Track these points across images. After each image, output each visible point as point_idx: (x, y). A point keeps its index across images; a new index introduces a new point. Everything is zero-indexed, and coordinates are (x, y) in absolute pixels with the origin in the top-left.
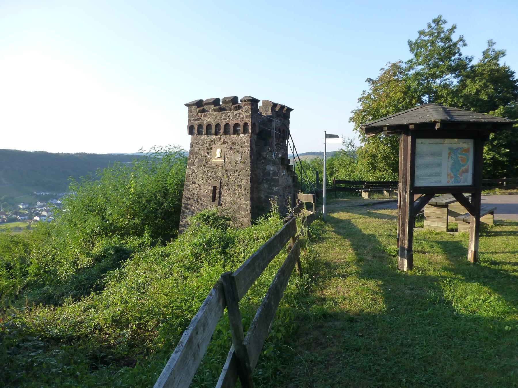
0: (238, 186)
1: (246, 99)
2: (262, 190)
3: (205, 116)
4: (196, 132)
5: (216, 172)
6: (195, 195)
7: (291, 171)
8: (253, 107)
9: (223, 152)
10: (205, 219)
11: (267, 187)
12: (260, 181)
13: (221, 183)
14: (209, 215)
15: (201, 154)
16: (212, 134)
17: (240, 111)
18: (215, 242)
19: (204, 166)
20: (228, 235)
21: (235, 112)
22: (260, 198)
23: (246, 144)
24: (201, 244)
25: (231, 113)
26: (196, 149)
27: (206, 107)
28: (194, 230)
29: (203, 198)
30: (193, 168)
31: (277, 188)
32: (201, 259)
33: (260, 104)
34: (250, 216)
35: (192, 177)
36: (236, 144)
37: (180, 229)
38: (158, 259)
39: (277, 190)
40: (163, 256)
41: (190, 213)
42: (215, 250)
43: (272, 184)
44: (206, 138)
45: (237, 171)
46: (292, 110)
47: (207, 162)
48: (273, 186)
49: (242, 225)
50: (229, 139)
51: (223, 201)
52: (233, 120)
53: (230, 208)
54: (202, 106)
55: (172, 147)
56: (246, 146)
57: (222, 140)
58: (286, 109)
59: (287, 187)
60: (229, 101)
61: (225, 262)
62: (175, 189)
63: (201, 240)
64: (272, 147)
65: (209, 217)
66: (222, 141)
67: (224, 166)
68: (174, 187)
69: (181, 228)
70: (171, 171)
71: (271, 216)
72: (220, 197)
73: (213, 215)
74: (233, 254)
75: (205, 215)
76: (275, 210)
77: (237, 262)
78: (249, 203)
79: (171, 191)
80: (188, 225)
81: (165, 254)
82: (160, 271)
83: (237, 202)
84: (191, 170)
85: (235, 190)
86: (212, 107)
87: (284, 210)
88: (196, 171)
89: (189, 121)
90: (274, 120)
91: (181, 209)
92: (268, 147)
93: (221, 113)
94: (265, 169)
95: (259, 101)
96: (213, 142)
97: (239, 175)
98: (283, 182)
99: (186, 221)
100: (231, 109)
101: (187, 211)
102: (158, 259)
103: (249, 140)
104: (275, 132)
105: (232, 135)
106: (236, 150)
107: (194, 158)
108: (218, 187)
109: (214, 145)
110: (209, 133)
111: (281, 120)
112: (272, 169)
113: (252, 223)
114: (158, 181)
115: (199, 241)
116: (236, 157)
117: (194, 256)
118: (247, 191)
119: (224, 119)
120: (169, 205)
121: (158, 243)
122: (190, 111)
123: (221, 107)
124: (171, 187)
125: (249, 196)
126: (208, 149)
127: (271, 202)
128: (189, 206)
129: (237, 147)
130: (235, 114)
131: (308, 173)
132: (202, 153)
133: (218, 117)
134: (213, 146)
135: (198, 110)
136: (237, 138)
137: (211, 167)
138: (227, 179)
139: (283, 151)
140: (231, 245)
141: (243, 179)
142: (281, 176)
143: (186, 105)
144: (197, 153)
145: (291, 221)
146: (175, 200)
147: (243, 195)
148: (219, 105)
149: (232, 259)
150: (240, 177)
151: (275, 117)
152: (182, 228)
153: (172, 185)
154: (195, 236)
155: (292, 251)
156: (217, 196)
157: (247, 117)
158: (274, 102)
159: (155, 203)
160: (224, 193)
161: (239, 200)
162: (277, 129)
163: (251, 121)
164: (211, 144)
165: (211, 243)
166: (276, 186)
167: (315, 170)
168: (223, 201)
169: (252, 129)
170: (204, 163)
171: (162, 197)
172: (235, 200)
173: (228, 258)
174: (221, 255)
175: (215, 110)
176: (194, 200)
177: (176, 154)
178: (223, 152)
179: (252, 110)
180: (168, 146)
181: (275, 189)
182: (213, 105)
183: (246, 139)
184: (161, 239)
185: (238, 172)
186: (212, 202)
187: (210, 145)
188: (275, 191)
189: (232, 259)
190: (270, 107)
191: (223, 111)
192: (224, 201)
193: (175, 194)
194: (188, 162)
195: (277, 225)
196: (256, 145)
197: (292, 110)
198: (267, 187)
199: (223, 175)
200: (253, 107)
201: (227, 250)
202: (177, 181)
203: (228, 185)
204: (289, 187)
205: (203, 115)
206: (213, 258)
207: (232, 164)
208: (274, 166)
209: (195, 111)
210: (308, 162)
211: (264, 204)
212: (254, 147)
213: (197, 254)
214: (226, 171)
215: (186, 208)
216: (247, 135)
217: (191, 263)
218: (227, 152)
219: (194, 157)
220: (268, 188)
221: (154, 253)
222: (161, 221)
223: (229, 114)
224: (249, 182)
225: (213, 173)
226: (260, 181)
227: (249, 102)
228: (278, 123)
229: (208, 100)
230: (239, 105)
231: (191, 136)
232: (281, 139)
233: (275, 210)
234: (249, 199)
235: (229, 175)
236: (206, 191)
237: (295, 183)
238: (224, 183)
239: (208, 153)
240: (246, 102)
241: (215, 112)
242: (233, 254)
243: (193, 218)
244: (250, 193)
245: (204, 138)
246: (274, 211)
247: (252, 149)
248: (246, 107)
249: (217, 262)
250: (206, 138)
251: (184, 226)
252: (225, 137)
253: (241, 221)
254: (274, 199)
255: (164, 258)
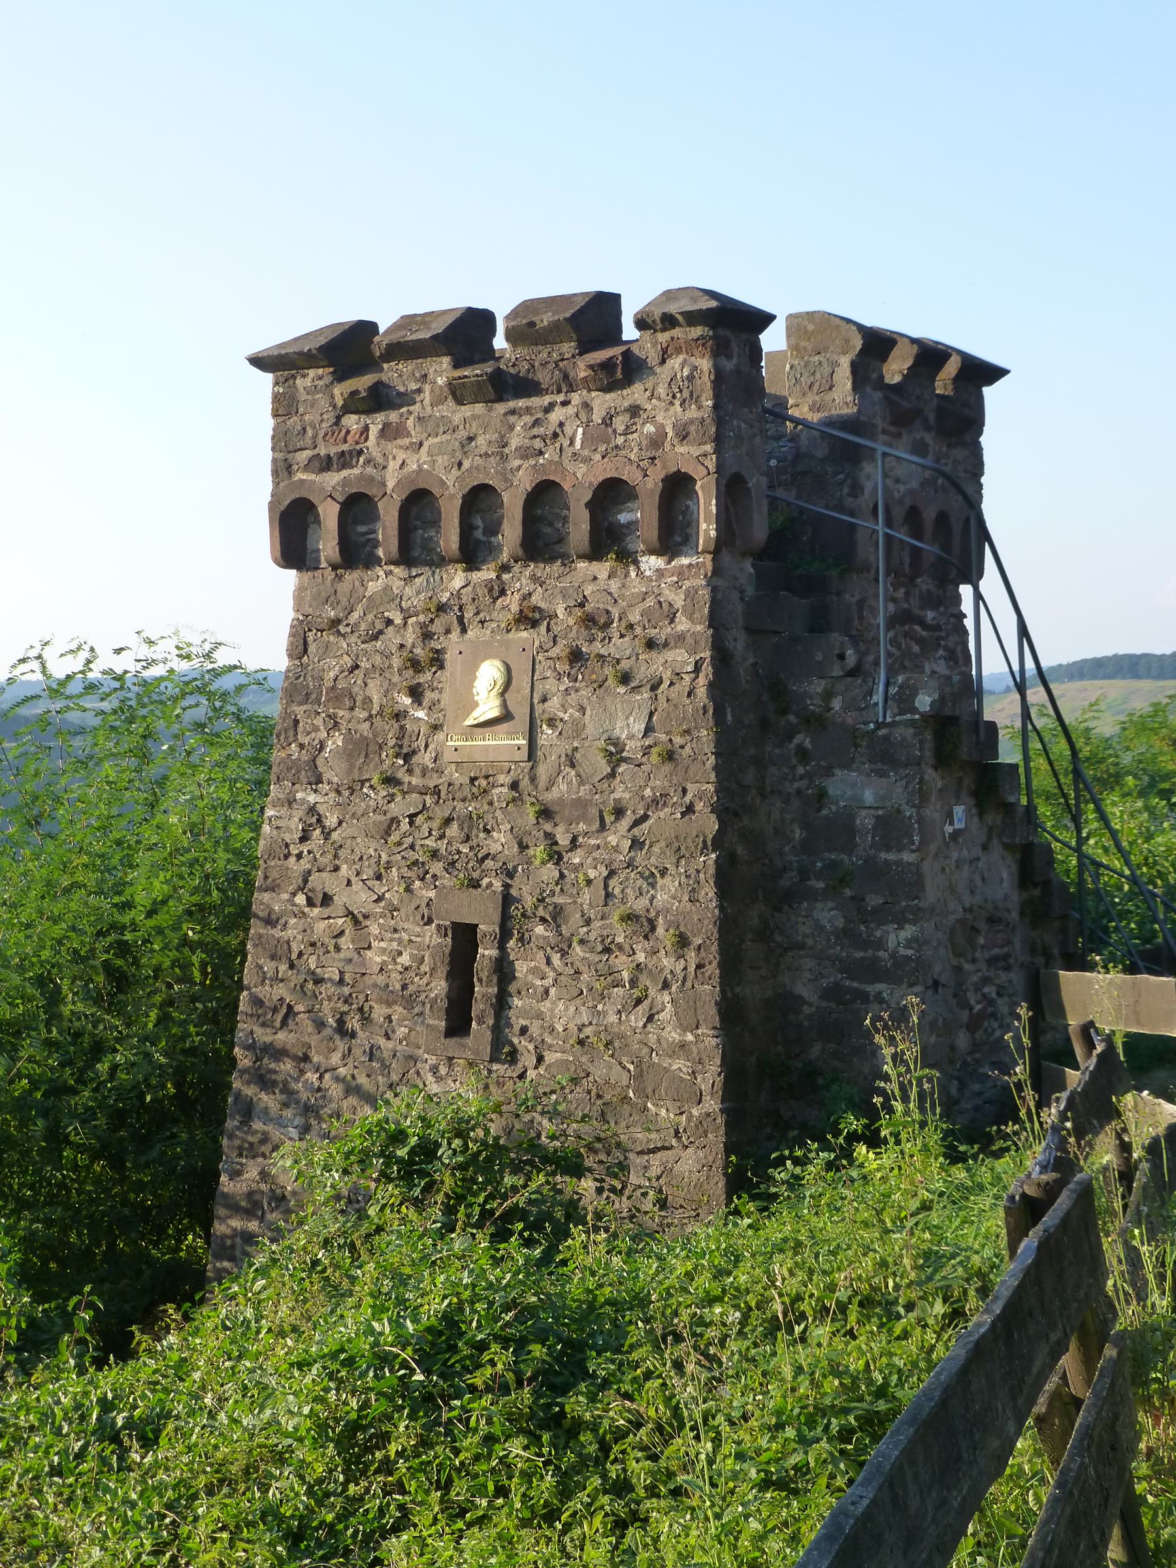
0: (629, 918)
1: (673, 308)
2: (801, 946)
3: (388, 433)
4: (327, 544)
5: (473, 826)
6: (326, 990)
7: (1009, 809)
8: (728, 365)
9: (522, 682)
10: (400, 1161)
11: (840, 923)
12: (784, 883)
13: (507, 899)
14: (434, 1135)
15: (368, 700)
16: (439, 562)
17: (636, 393)
18: (482, 1347)
19: (389, 780)
20: (574, 1290)
21: (602, 402)
22: (787, 1002)
23: (683, 624)
24: (383, 1360)
25: (571, 410)
26: (332, 668)
27: (397, 374)
28: (326, 1243)
29: (379, 1012)
30: (312, 798)
31: (908, 932)
32: (387, 1467)
33: (773, 340)
34: (717, 1138)
35: (305, 864)
36: (608, 624)
37: (219, 1228)
38: (80, 1456)
39: (909, 944)
40: (115, 1439)
41: (288, 1113)
42: (487, 1400)
43: (874, 901)
44: (397, 585)
45: (619, 812)
46: (994, 373)
47: (407, 757)
48: (881, 915)
49: (663, 1204)
50: (564, 594)
51: (524, 1030)
52: (587, 460)
53: (575, 1081)
54: (367, 363)
55: (167, 647)
56: (681, 637)
57: (512, 602)
58: (952, 367)
59: (982, 925)
60: (555, 326)
61: (565, 1492)
62: (185, 942)
63: (383, 1326)
64: (863, 640)
65: (427, 1150)
66: (515, 608)
67: (525, 783)
68: (176, 927)
69: (226, 1225)
70: (159, 818)
71: (874, 1141)
72: (501, 1003)
73: (459, 1134)
74: (620, 1435)
75: (399, 1137)
76: (905, 1099)
77: (652, 1492)
78: (709, 1040)
79: (157, 955)
80: (279, 1200)
81: (129, 1424)
82: (96, 1552)
83: (621, 1036)
84: (298, 813)
85: (607, 950)
86: (441, 370)
87: (962, 1086)
88: (331, 821)
89: (282, 469)
90: (880, 449)
91: (229, 1086)
92: (836, 638)
93: (501, 408)
94: (822, 794)
95: (765, 319)
96: (451, 617)
97: (636, 844)
98: (952, 889)
99: (264, 1175)
100: (568, 383)
101: (268, 1100)
102: (80, 1456)
103: (704, 594)
104: (887, 535)
105: (582, 565)
106: (608, 671)
107: (314, 726)
108: (487, 927)
109: (455, 635)
110: (416, 553)
111: (920, 448)
112: (868, 796)
113: (737, 1184)
114: (67, 891)
115: (371, 1331)
116: (612, 718)
117: (338, 1443)
118: (692, 957)
119: (526, 453)
120: (148, 1056)
121: (69, 1327)
122: (284, 406)
123: (498, 370)
124: (160, 931)
125: (708, 991)
126: (415, 665)
127: (879, 1039)
128: (287, 1067)
129: (619, 646)
130: (597, 418)
131: (1116, 807)
132: (375, 692)
133: (481, 441)
134: (453, 644)
135: (340, 391)
136: (614, 586)
137: (436, 791)
138: (550, 872)
139: (941, 668)
140: (599, 1365)
141: (664, 872)
142: (933, 847)
143: (258, 361)
144: (338, 696)
145: (1064, 1201)
146: (183, 1024)
147: (666, 985)
148: (489, 353)
149: (613, 1471)
150: (640, 857)
151: (880, 424)
152: (236, 1223)
153: (161, 919)
154: (336, 1294)
155: (1087, 1432)
156: (483, 991)
157: (683, 436)
158: (869, 322)
159: (50, 1044)
160: (534, 971)
161: (637, 1018)
162: (899, 513)
163: (711, 462)
164: (437, 627)
165: (453, 1349)
166: (901, 921)
167: (1152, 784)
168: (524, 1030)
169: (725, 521)
170: (389, 761)
171: (97, 1000)
172: (613, 1018)
173: (583, 1462)
174: (535, 1439)
175: (458, 393)
176: (320, 1025)
177: (189, 701)
178: (522, 682)
179: (719, 380)
180: (133, 641)
181: (892, 942)
182: (446, 361)
183: (677, 585)
184: (91, 1305)
185: (625, 823)
186: (450, 1032)
187: (427, 636)
188: (894, 956)
189: (613, 1471)
190: (845, 362)
191: (518, 395)
192: (534, 1030)
193: (187, 979)
194: (277, 755)
195: (926, 1207)
196: (749, 630)
197: (994, 373)
198: (840, 923)
199: (523, 847)
200: (728, 365)
201: (576, 1404)
202: (195, 891)
203: (557, 915)
204: (992, 920)
205: (374, 431)
206: (477, 1458)
207: (585, 768)
208: (882, 774)
209: (322, 401)
210: (1106, 727)
211: (815, 1051)
212: (738, 642)
213: (354, 1427)
214: (545, 813)
215: (265, 1081)
216: (685, 561)
217: (319, 1493)
218: (551, 685)
219: (319, 721)
220: (846, 934)
221: (46, 1416)
222: (88, 1168)
223: (556, 415)
224: (708, 892)
225: (453, 830)
226: (784, 883)
227: (697, 331)
228: (900, 472)
229: (408, 322)
230: (627, 355)
231: (292, 574)
232: (925, 584)
233: (905, 1099)
234: (711, 1013)
235: (563, 840)
236: (405, 959)
237: (1037, 892)
238: (529, 901)
239: (416, 693)
240: (676, 332)
241: (460, 402)
242: (620, 1435)
243: (319, 1157)
244: (713, 969)
245: (387, 588)
246: (898, 1106)
247: (722, 657)
248: (675, 362)
249: (502, 1491)
250: (397, 585)
251: (252, 1207)
252: (534, 578)
253: (654, 1171)
254: (901, 1015)
255: (122, 1455)
